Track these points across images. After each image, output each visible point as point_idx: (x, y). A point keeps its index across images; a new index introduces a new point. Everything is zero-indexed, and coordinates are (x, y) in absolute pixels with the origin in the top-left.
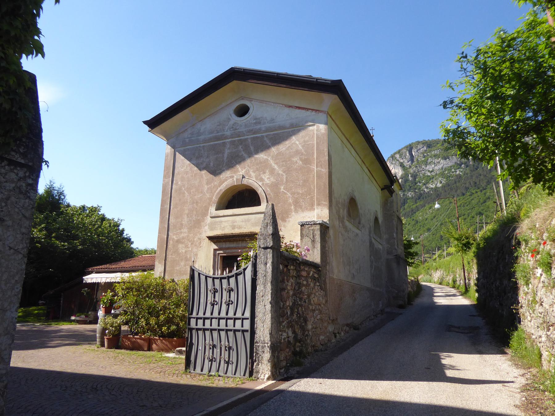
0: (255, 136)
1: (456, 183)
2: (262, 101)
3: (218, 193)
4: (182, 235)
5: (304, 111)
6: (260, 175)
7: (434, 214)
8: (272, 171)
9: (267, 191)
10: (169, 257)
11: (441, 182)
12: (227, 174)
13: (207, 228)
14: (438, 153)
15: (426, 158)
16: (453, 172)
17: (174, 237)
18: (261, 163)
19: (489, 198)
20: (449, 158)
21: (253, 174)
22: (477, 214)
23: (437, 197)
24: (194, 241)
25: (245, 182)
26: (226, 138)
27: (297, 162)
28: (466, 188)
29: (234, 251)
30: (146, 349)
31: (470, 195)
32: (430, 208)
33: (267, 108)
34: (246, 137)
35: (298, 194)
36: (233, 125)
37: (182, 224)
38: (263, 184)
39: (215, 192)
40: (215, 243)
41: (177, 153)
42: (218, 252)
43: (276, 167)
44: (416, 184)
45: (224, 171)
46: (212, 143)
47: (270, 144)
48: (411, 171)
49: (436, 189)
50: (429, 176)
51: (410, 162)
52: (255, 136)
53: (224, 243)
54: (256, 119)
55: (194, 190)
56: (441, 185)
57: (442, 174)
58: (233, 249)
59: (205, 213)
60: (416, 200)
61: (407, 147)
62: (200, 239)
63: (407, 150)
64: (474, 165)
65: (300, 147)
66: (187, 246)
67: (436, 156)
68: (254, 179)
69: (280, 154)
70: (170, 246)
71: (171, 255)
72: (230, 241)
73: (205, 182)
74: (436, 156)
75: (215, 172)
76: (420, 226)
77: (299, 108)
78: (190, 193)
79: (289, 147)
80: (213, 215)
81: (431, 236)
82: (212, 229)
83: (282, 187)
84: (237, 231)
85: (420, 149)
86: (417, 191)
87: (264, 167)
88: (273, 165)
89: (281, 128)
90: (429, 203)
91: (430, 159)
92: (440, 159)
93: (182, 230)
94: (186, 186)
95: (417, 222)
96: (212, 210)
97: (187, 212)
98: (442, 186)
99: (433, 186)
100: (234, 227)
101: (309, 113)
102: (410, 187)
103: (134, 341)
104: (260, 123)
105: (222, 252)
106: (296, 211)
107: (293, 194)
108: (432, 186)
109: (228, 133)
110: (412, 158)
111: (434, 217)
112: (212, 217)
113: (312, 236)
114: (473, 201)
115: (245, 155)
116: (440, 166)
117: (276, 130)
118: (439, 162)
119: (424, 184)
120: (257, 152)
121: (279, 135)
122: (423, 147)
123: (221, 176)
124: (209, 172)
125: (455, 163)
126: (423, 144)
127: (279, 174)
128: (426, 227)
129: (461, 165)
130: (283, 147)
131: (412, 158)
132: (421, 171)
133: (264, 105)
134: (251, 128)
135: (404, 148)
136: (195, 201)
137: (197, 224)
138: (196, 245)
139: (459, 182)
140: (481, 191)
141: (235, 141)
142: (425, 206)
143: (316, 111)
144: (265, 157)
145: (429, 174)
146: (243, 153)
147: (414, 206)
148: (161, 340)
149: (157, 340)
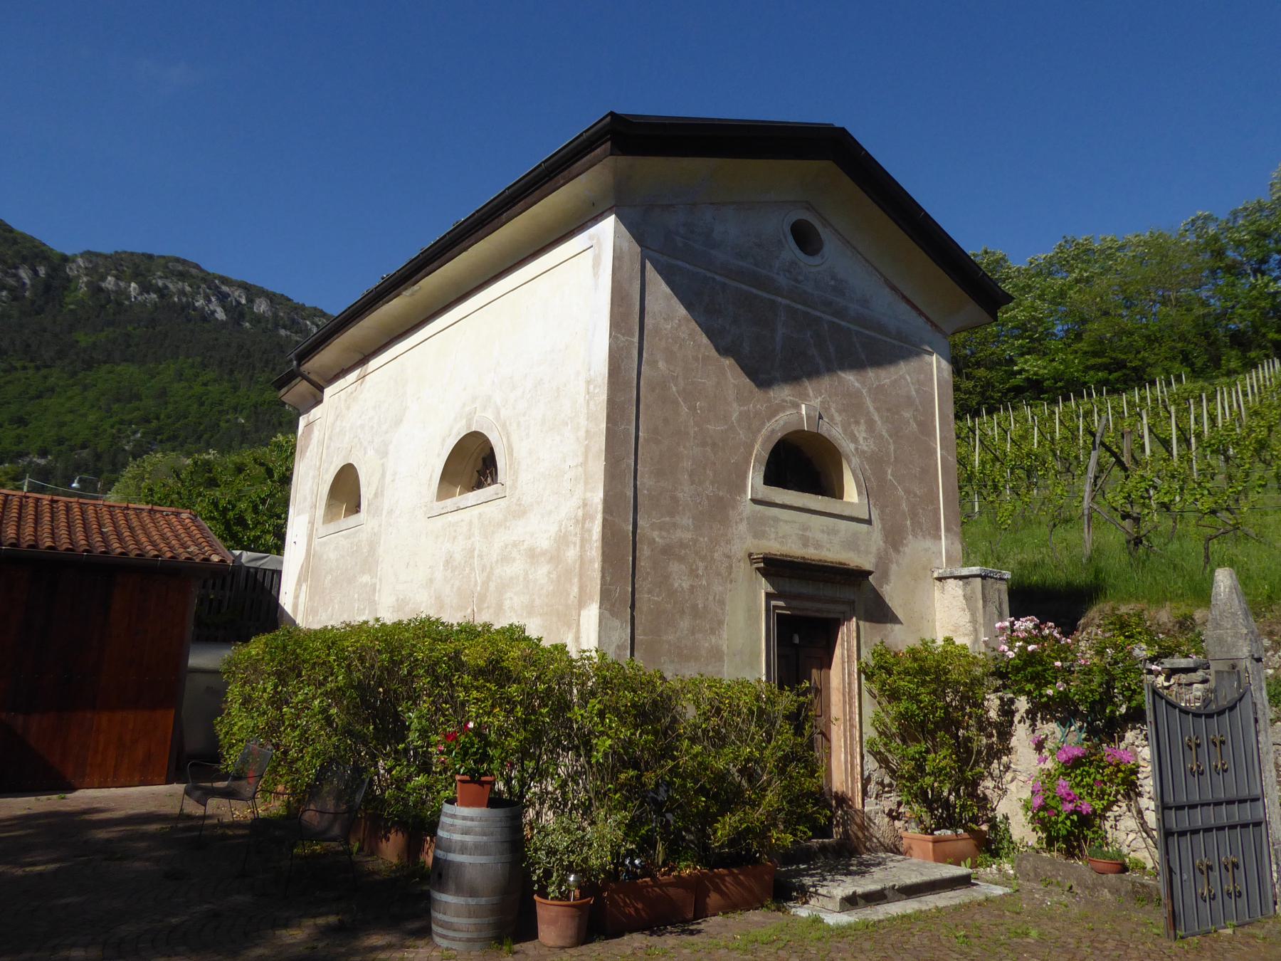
3: (768, 438)
5: (914, 313)
6: (849, 424)
8: (871, 424)
10: (642, 597)
12: (783, 393)
13: (743, 527)
17: (655, 534)
19: (52, 390)
21: (838, 418)
25: (825, 429)
29: (808, 605)
30: (691, 916)
33: (854, 267)
34: (818, 314)
35: (915, 495)
37: (675, 499)
38: (856, 449)
39: (759, 431)
42: (773, 603)
43: (876, 417)
46: (744, 287)
54: (833, 277)
62: (729, 557)
64: (33, 302)
66: (693, 573)
70: (643, 563)
71: (650, 592)
77: (908, 302)
80: (759, 496)
82: (758, 535)
84: (811, 553)
88: (871, 409)
96: (754, 480)
97: (687, 464)
100: (805, 542)
101: (921, 321)
105: (781, 603)
107: (907, 492)
109: (782, 280)
137: (717, 510)
138: (719, 574)
140: (38, 368)
143: (933, 324)
144: (857, 384)
148: (735, 876)
149: (722, 877)
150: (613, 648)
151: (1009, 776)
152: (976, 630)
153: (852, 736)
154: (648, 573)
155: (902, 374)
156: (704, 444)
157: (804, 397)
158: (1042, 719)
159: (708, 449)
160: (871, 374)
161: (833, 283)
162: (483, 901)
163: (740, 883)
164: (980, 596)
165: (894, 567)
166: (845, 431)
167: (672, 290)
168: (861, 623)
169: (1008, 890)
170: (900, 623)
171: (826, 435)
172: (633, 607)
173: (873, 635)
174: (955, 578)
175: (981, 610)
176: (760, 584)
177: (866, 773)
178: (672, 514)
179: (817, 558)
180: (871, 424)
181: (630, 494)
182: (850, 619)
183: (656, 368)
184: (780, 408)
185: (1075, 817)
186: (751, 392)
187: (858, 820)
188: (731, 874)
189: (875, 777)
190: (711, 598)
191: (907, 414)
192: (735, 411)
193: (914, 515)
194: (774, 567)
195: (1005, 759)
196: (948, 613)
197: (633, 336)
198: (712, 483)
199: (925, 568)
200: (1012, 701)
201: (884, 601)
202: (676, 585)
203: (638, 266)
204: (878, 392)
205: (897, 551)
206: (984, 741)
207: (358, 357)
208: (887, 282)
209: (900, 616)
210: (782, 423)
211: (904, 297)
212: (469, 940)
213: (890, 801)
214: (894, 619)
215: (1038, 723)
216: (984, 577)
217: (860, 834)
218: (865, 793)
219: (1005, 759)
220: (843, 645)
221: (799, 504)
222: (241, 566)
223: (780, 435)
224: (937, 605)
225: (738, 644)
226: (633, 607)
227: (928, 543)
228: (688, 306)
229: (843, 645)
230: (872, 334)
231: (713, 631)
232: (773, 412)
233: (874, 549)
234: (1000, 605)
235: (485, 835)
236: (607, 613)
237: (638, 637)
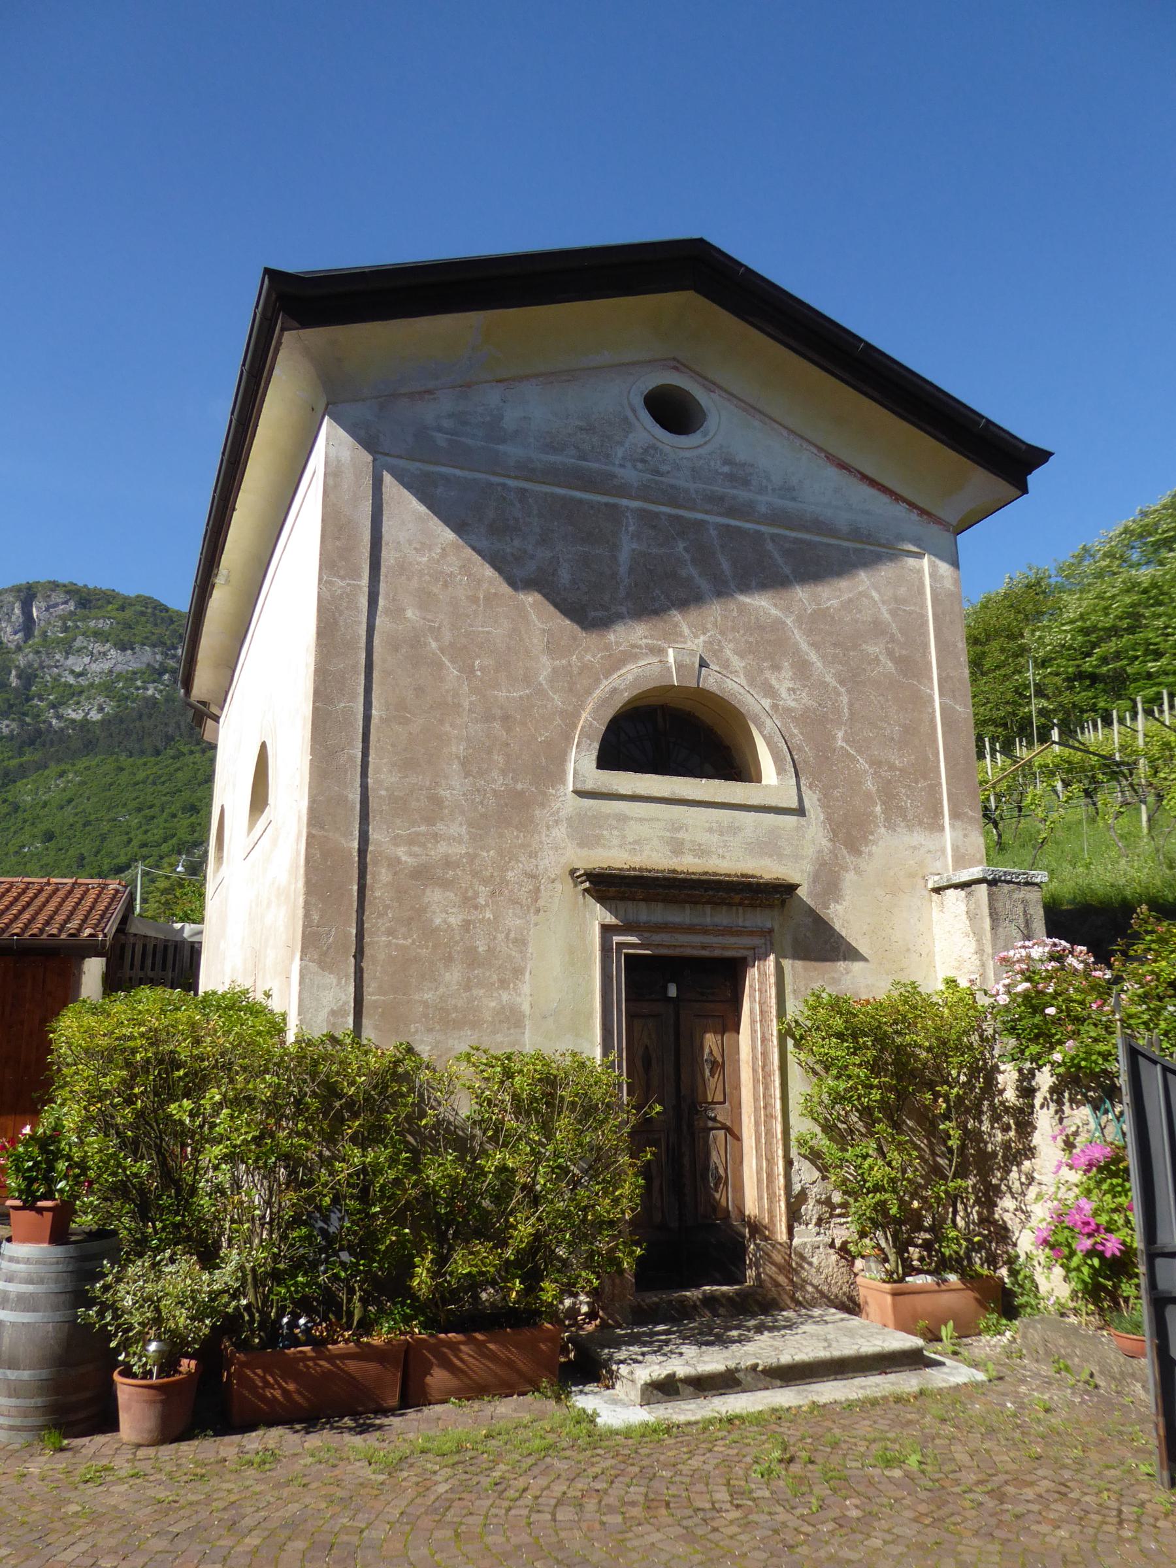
0: (733, 522)
1: (140, 717)
2: (753, 409)
3: (604, 702)
4: (442, 848)
5: (885, 499)
6: (761, 671)
7: (68, 795)
8: (802, 669)
9: (792, 735)
10: (379, 943)
11: (101, 709)
12: (632, 634)
13: (560, 833)
14: (107, 628)
15: (71, 635)
16: (138, 688)
17: (401, 852)
18: (761, 628)
20: (133, 649)
21: (737, 663)
22: (184, 810)
23: (86, 746)
24: (504, 881)
25: (711, 681)
26: (623, 491)
27: (877, 659)
28: (167, 736)
30: (394, 1402)
31: (173, 758)
32: (61, 776)
33: (766, 439)
34: (699, 516)
35: (892, 767)
36: (646, 451)
37: (437, 801)
38: (775, 707)
39: (589, 692)
40: (601, 899)
41: (387, 478)
42: (616, 939)
43: (813, 657)
44: (28, 699)
45: (619, 617)
47: (787, 570)
48: (21, 661)
49: (85, 724)
50: (71, 686)
51: (20, 635)
52: (733, 522)
53: (643, 905)
54: (727, 461)
55: (489, 662)
56: (99, 717)
57: (107, 689)
58: (696, 935)
59: (549, 770)
60: (21, 747)
61: (17, 590)
62: (534, 877)
63: (18, 598)
65: (886, 616)
66: (469, 902)
67: (97, 634)
68: (744, 683)
69: (821, 615)
71: (390, 932)
72: (666, 900)
73: (537, 642)
74: (97, 634)
75: (589, 609)
76: (25, 821)
78: (468, 671)
79: (850, 600)
80: (589, 786)
81: (53, 853)
82: (586, 842)
83: (840, 735)
84: (689, 864)
85: (56, 605)
86: (28, 720)
87: (769, 646)
88: (804, 646)
89: (820, 526)
90: (59, 761)
91: (80, 638)
92: (108, 645)
93: (440, 827)
94: (447, 636)
95: (16, 808)
96: (581, 763)
97: (459, 749)
98: (102, 722)
99: (77, 716)
100: (678, 848)
101: (900, 510)
102: (11, 706)
103: (326, 1374)
104: (746, 483)
105: (633, 939)
106: (891, 826)
107: (876, 763)
108: (73, 715)
109: (630, 475)
110: (28, 625)
111: (70, 801)
112: (580, 794)
113: (1021, 921)
114: (179, 774)
115: (704, 585)
116: (107, 666)
117: (807, 530)
118: (105, 654)
119: (53, 706)
120: (745, 588)
121: (815, 554)
122: (66, 603)
123: (612, 637)
124: (556, 605)
125: (148, 665)
126: (68, 592)
127: (825, 685)
128: (42, 827)
129: (161, 674)
130: (831, 595)
131: (28, 625)
132: (50, 667)
133: (757, 423)
134: (718, 489)
135: (11, 590)
136: (498, 712)
137: (517, 810)
138: (515, 902)
139: (150, 716)
141: (657, 515)
142: (46, 767)
143: (923, 512)
144: (774, 612)
145: (71, 680)
146: (693, 571)
147: (14, 762)
148: (480, 1345)
149: (454, 1346)
150: (323, 1014)
151: (1033, 1191)
152: (983, 965)
153: (769, 1132)
154: (387, 907)
155: (866, 591)
156: (488, 718)
157: (673, 636)
158: (1071, 1101)
159: (496, 725)
160: (801, 594)
161: (726, 469)
162: (26, 1375)
163: (493, 1357)
164: (985, 911)
165: (849, 877)
166: (752, 681)
167: (429, 508)
168: (787, 963)
169: (981, 1376)
170: (865, 960)
171: (714, 689)
172: (359, 954)
173: (807, 981)
174: (957, 886)
175: (988, 934)
176: (593, 912)
177: (797, 1188)
178: (430, 821)
179: (700, 870)
180: (802, 669)
181: (355, 796)
182: (765, 957)
183: (403, 614)
184: (629, 656)
185: (1096, 1262)
186: (575, 639)
187: (778, 1258)
188: (471, 1341)
189: (814, 1192)
190: (500, 937)
191: (873, 649)
192: (545, 667)
193: (888, 795)
194: (604, 885)
195: (1027, 1163)
196: (937, 936)
197: (359, 577)
198: (504, 773)
199: (912, 876)
200: (1032, 1073)
201: (832, 928)
202: (438, 921)
203: (368, 482)
204: (815, 622)
205: (857, 852)
206: (999, 1137)
207: (230, 672)
208: (832, 459)
209: (863, 950)
210: (630, 677)
211: (864, 477)
212: (11, 1428)
213: (844, 1231)
214: (852, 954)
215: (1066, 1108)
216: (993, 883)
217: (782, 1279)
218: (794, 1216)
219: (1027, 1163)
220: (752, 996)
221: (665, 793)
222: (184, 941)
223: (626, 696)
224: (936, 930)
225: (557, 1000)
226: (359, 954)
227: (918, 838)
228: (459, 528)
229: (752, 996)
230: (800, 535)
231: (504, 984)
232: (617, 662)
233: (810, 851)
234: (1027, 923)
235: (31, 1282)
236: (313, 967)
237: (368, 998)
